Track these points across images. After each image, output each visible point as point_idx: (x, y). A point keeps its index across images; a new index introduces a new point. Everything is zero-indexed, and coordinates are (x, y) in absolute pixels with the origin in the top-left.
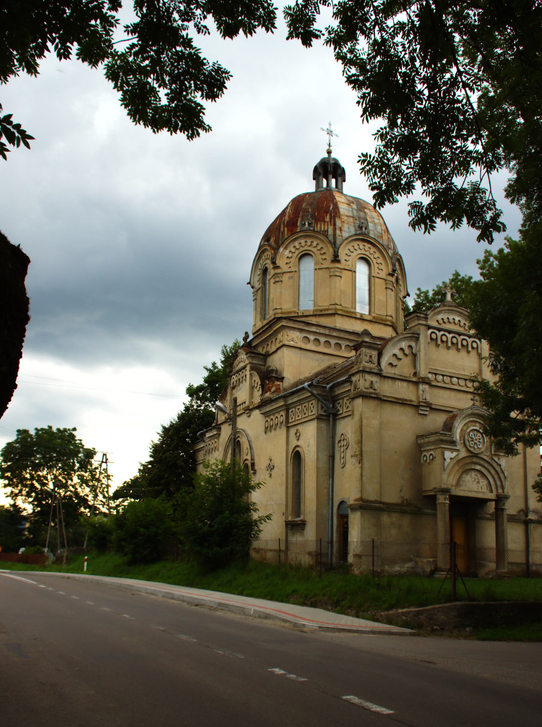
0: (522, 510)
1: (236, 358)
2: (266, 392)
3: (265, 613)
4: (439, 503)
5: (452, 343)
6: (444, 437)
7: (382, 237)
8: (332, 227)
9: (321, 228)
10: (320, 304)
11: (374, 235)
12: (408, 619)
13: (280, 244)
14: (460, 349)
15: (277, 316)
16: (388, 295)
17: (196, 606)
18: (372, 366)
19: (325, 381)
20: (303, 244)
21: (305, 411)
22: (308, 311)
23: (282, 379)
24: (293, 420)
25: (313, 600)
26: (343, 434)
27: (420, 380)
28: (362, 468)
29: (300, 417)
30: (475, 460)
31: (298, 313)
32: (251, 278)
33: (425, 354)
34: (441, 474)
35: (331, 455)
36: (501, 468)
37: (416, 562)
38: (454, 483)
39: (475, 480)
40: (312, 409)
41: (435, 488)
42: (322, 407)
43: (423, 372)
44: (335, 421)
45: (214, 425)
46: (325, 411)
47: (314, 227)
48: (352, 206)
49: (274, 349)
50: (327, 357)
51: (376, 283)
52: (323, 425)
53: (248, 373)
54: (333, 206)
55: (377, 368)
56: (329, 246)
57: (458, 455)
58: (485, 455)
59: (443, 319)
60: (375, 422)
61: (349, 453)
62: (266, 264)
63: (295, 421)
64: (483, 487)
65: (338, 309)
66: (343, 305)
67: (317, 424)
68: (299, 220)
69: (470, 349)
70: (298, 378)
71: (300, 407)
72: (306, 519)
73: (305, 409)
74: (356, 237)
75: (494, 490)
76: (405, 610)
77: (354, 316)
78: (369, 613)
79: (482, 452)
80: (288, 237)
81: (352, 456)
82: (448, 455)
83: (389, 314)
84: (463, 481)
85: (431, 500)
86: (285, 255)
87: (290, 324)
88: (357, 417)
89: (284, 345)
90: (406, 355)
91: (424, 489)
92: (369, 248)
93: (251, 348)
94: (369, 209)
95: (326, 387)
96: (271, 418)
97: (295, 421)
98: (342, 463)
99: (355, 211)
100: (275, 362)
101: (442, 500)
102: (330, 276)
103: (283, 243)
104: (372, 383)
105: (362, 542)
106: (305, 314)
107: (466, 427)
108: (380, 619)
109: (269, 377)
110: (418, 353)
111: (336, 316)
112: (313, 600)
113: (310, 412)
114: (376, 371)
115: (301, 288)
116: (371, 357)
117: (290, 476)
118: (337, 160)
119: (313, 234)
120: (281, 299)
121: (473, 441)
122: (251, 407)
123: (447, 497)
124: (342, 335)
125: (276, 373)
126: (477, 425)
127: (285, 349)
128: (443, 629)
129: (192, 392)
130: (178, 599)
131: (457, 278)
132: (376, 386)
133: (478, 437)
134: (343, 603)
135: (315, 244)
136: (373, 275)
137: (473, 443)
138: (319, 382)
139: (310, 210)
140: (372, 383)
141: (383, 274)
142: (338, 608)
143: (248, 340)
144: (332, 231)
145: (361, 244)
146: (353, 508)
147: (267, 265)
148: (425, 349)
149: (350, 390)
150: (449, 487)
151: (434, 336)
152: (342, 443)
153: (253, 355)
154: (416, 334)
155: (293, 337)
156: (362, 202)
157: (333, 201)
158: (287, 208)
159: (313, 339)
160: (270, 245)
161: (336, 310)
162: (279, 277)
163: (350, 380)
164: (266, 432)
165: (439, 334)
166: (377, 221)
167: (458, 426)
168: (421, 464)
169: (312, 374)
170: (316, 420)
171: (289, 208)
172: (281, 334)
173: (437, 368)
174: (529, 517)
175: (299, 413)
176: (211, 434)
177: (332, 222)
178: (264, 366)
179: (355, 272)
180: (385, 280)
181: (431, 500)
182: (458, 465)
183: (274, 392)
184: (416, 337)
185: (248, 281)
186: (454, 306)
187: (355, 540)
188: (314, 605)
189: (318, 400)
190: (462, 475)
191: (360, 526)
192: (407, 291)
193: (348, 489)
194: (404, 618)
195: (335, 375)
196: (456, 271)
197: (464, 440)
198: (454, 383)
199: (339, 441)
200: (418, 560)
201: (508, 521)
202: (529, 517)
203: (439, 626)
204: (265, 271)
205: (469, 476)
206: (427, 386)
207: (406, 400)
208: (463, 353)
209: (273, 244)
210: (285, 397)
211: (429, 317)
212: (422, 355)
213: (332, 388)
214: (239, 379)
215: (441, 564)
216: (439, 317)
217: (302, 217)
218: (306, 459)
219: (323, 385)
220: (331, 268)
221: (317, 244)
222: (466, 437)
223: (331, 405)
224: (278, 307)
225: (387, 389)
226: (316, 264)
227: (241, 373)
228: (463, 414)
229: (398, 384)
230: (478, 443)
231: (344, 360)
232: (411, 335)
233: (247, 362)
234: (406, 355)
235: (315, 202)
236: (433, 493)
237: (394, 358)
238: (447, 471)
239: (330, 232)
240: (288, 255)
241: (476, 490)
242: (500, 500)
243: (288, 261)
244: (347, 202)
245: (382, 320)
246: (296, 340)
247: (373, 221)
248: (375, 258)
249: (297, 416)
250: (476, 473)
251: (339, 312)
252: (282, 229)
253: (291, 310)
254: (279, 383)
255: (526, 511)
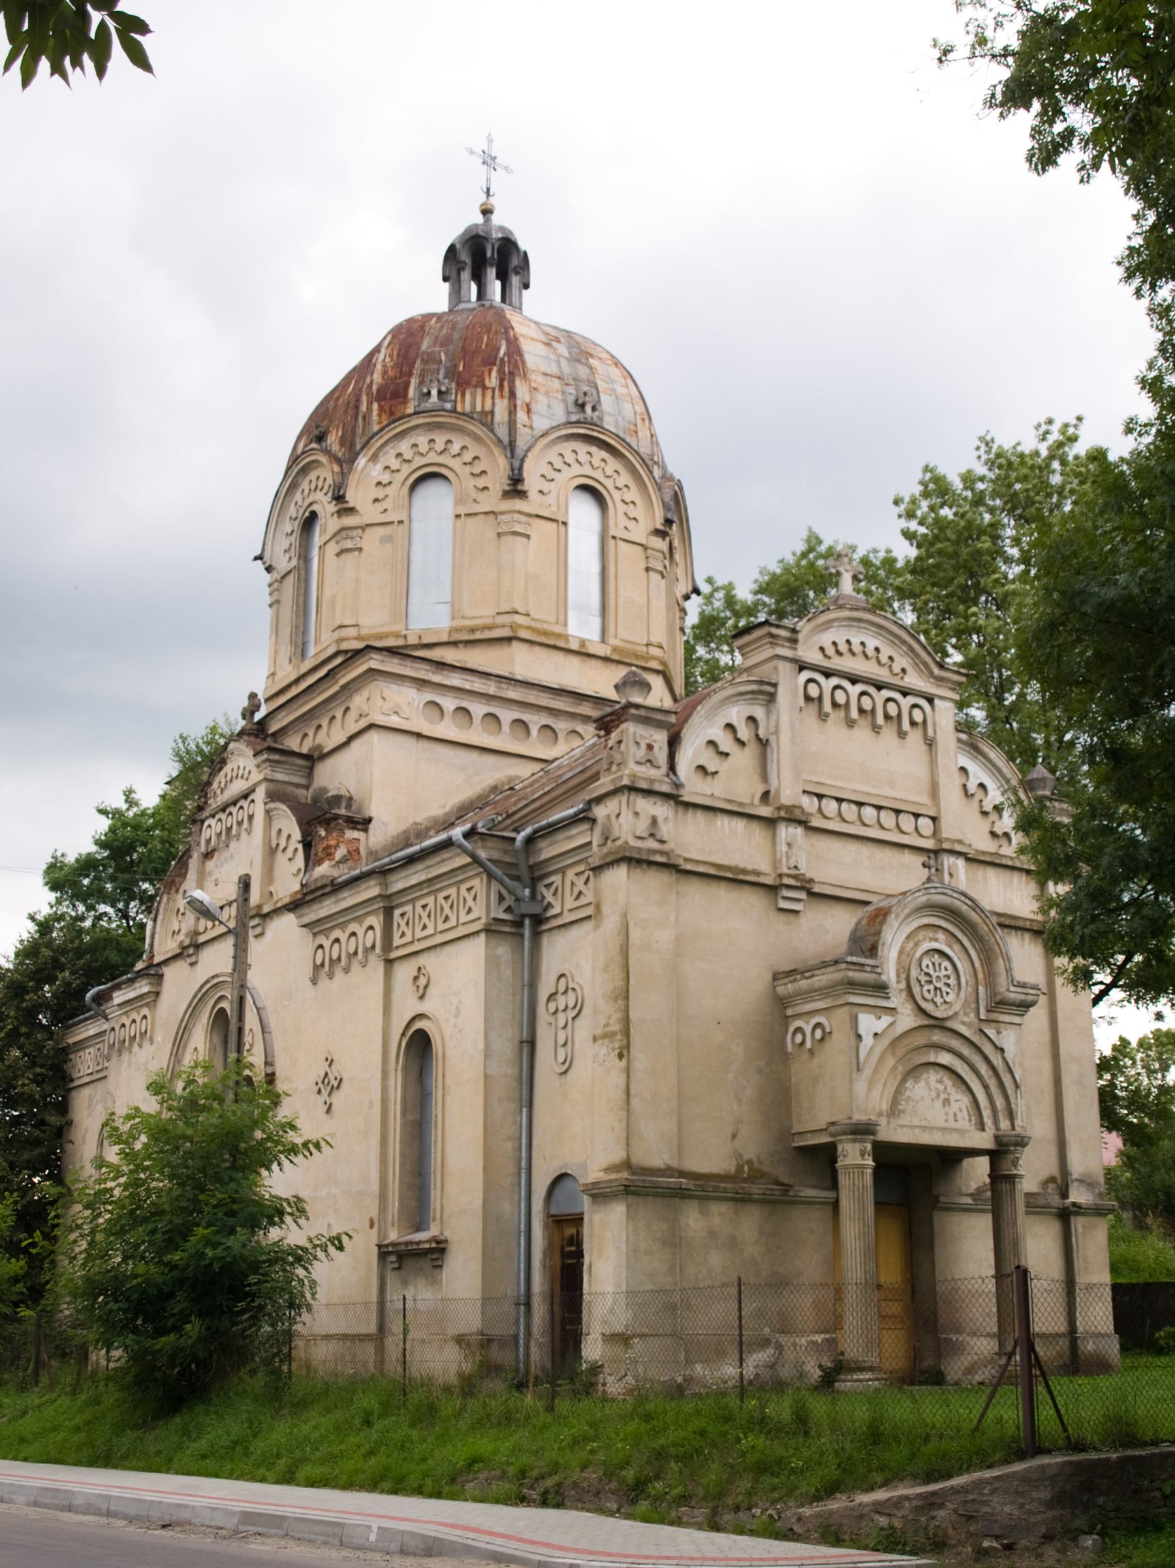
0: (1052, 1179)
1: (221, 769)
2: (319, 862)
3: (425, 1537)
4: (846, 1167)
5: (861, 711)
6: (855, 971)
7: (636, 432)
8: (506, 401)
9: (473, 405)
10: (469, 613)
11: (616, 426)
12: (897, 1523)
13: (358, 447)
14: (880, 727)
15: (345, 646)
16: (652, 586)
17: (164, 1527)
18: (653, 773)
19: (509, 821)
20: (423, 448)
21: (447, 911)
22: (437, 632)
23: (364, 823)
24: (408, 938)
25: (549, 1483)
26: (562, 975)
27: (782, 814)
28: (628, 1071)
29: (430, 930)
30: (937, 1037)
31: (405, 637)
32: (264, 544)
33: (793, 742)
34: (851, 1081)
35: (525, 1037)
36: (1004, 1058)
37: (779, 1347)
38: (885, 1107)
39: (938, 1095)
40: (470, 902)
41: (833, 1124)
42: (501, 898)
43: (789, 793)
44: (537, 935)
45: (140, 966)
46: (509, 910)
47: (455, 401)
48: (555, 349)
49: (339, 737)
50: (490, 759)
51: (620, 555)
52: (503, 950)
53: (259, 809)
54: (508, 347)
55: (667, 780)
56: (497, 451)
57: (893, 1024)
58: (963, 1023)
59: (834, 643)
60: (664, 937)
61: (583, 1030)
62: (311, 504)
63: (412, 942)
64: (959, 1115)
65: (521, 626)
66: (533, 615)
67: (487, 946)
68: (414, 382)
69: (906, 725)
70: (411, 821)
71: (430, 900)
72: (447, 1234)
73: (446, 906)
74: (570, 431)
75: (988, 1121)
76: (881, 1495)
77: (562, 644)
78: (757, 1512)
79: (956, 1014)
80: (381, 430)
81: (595, 1039)
82: (868, 1024)
83: (654, 640)
84: (908, 1099)
85: (821, 1160)
86: (369, 478)
87: (393, 665)
88: (611, 922)
89: (371, 726)
90: (742, 743)
91: (797, 1128)
92: (603, 460)
93: (264, 739)
94: (600, 359)
95: (514, 839)
96: (333, 936)
97: (412, 942)
98: (561, 1059)
99: (564, 363)
100: (336, 776)
101: (855, 1158)
102: (499, 535)
103: (366, 444)
104: (654, 821)
105: (631, 1293)
106: (425, 641)
107: (911, 944)
108: (798, 1529)
109: (325, 819)
110: (773, 739)
111: (515, 643)
112: (549, 1483)
113: (462, 913)
114: (665, 788)
115: (414, 568)
116: (650, 747)
117: (396, 1108)
118: (511, 233)
119: (454, 421)
120: (354, 598)
121: (930, 982)
122: (266, 909)
123: (869, 1146)
124: (532, 697)
125: (349, 806)
126: (941, 936)
127: (373, 736)
128: (1009, 1547)
129: (60, 878)
130: (90, 1509)
131: (811, 550)
132: (665, 830)
133: (944, 972)
134: (659, 1485)
135: (456, 448)
136: (612, 532)
137: (931, 987)
138: (493, 825)
139: (443, 357)
140: (654, 821)
141: (639, 532)
142: (644, 1505)
143: (258, 716)
144: (506, 414)
145: (582, 448)
146: (600, 1194)
147: (315, 508)
148: (793, 728)
149: (590, 843)
150: (873, 1118)
151: (813, 691)
152: (561, 1001)
153: (276, 757)
154: (769, 684)
155: (396, 702)
156: (578, 339)
157: (506, 332)
158: (377, 350)
159: (452, 708)
160: (327, 452)
161: (513, 627)
162: (352, 538)
163: (590, 815)
164: (314, 981)
165: (828, 684)
166: (621, 390)
167: (893, 939)
168: (786, 1054)
169: (447, 809)
170: (483, 936)
171: (383, 350)
172: (365, 693)
173: (822, 781)
174: (1072, 1199)
175: (425, 920)
176: (131, 995)
177: (506, 390)
178: (307, 787)
179: (565, 524)
180: (645, 548)
181: (821, 1160)
182: (893, 1053)
183: (343, 860)
184: (767, 694)
185: (258, 553)
186: (864, 609)
187: (610, 1289)
188: (552, 1499)
189: (491, 876)
190: (904, 1080)
191: (623, 1247)
192: (693, 579)
193: (582, 1134)
194: (883, 1521)
195: (537, 804)
196: (810, 529)
197: (908, 980)
198: (866, 821)
199: (552, 997)
200: (783, 1339)
201: (1027, 1213)
202: (1072, 1199)
203: (997, 1537)
204: (310, 521)
205: (922, 1083)
206: (800, 831)
207: (744, 871)
208: (889, 734)
209: (335, 448)
210: (383, 873)
211: (801, 636)
212: (783, 747)
213: (530, 840)
214: (229, 830)
215: (853, 1346)
216: (826, 639)
217: (422, 375)
218: (450, 1053)
219: (505, 834)
220: (503, 513)
221: (464, 448)
222: (914, 973)
223: (527, 892)
224: (346, 622)
225: (693, 839)
226: (459, 501)
227: (234, 810)
228: (905, 908)
229: (724, 823)
230: (945, 989)
231: (537, 766)
232: (754, 687)
233: (256, 777)
234: (742, 743)
235: (456, 336)
236: (825, 1139)
237: (711, 752)
238: (867, 1072)
239: (501, 415)
240: (380, 478)
241: (943, 1124)
242: (1002, 1153)
243: (380, 493)
244: (543, 338)
245: (637, 656)
246: (406, 711)
247: (613, 390)
248: (617, 488)
249: (418, 928)
250: (942, 1074)
251: (523, 634)
252: (364, 408)
253: (386, 629)
254: (356, 834)
255: (1062, 1182)
